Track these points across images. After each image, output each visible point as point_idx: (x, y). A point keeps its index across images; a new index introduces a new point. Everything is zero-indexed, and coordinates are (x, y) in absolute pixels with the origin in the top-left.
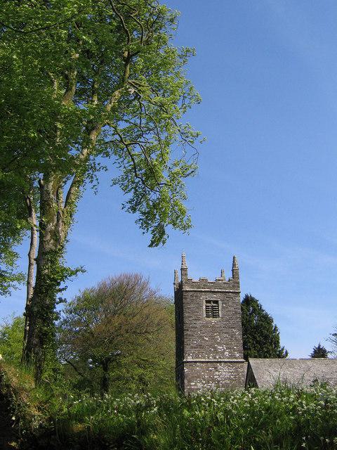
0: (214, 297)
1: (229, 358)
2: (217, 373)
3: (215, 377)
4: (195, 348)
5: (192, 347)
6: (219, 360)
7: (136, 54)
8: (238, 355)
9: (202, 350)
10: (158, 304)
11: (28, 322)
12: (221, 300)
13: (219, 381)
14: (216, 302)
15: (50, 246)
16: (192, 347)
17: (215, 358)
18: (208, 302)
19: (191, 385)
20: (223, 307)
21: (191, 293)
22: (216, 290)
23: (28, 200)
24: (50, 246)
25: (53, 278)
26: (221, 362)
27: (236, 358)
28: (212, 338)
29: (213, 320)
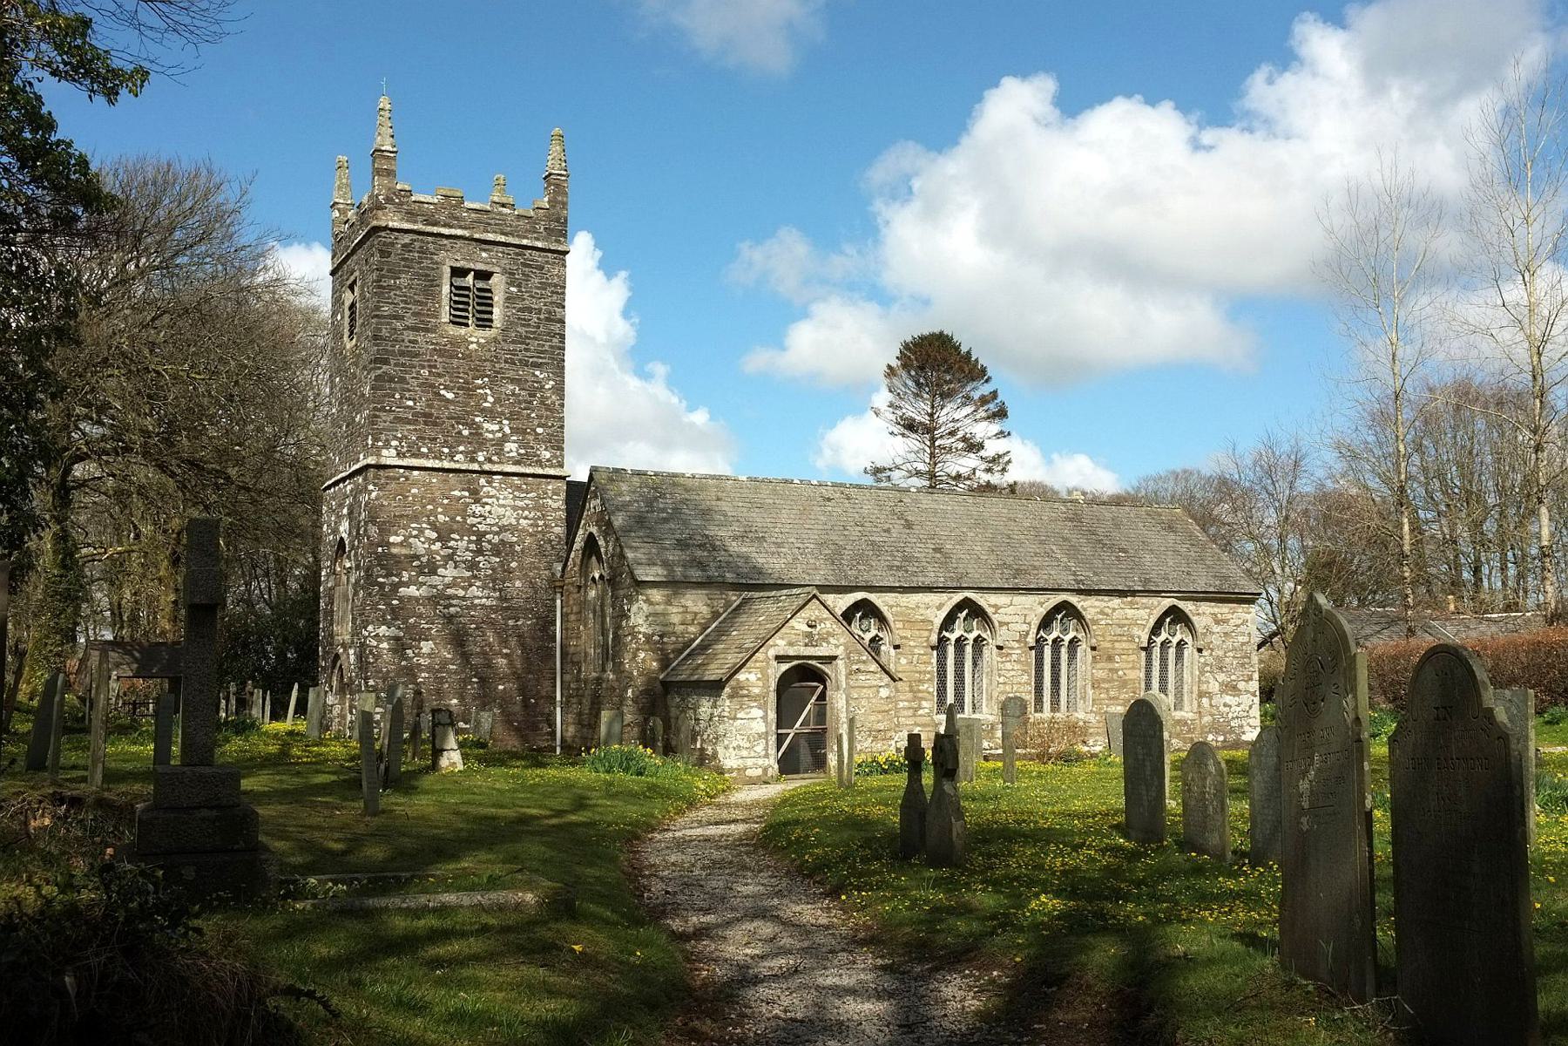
1: (517, 463)
2: (478, 509)
5: (398, 420)
6: (487, 467)
8: (547, 455)
9: (429, 432)
10: (309, 315)
12: (504, 272)
14: (484, 276)
15: (657, 723)
16: (398, 420)
18: (458, 272)
19: (389, 544)
21: (407, 239)
22: (491, 237)
23: (458, 537)
24: (657, 723)
25: (414, 626)
27: (540, 463)
29: (475, 336)
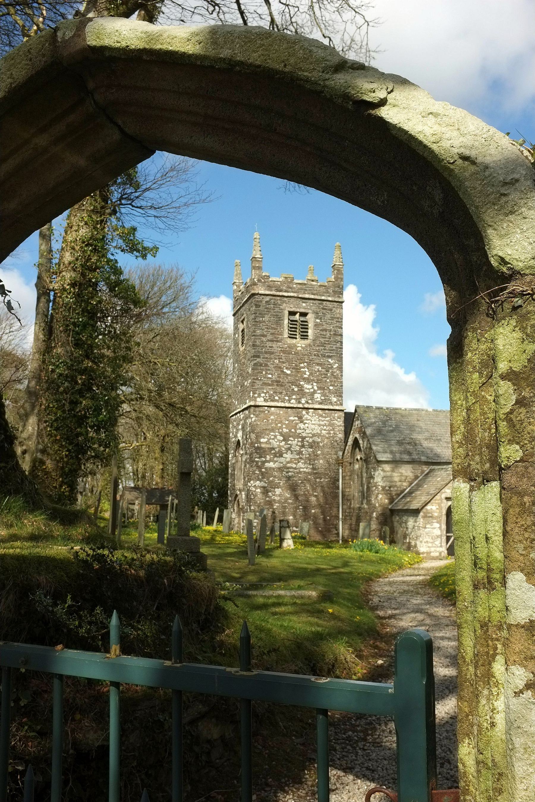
0: (303, 307)
1: (320, 403)
3: (298, 431)
4: (269, 385)
6: (306, 406)
7: (483, 384)
11: (298, 601)
13: (303, 438)
15: (387, 529)
16: (265, 384)
17: (300, 402)
18: (292, 313)
20: (316, 325)
21: (268, 298)
22: (307, 296)
24: (387, 529)
26: (308, 408)
27: (331, 403)
28: (297, 369)
29: (300, 344)
